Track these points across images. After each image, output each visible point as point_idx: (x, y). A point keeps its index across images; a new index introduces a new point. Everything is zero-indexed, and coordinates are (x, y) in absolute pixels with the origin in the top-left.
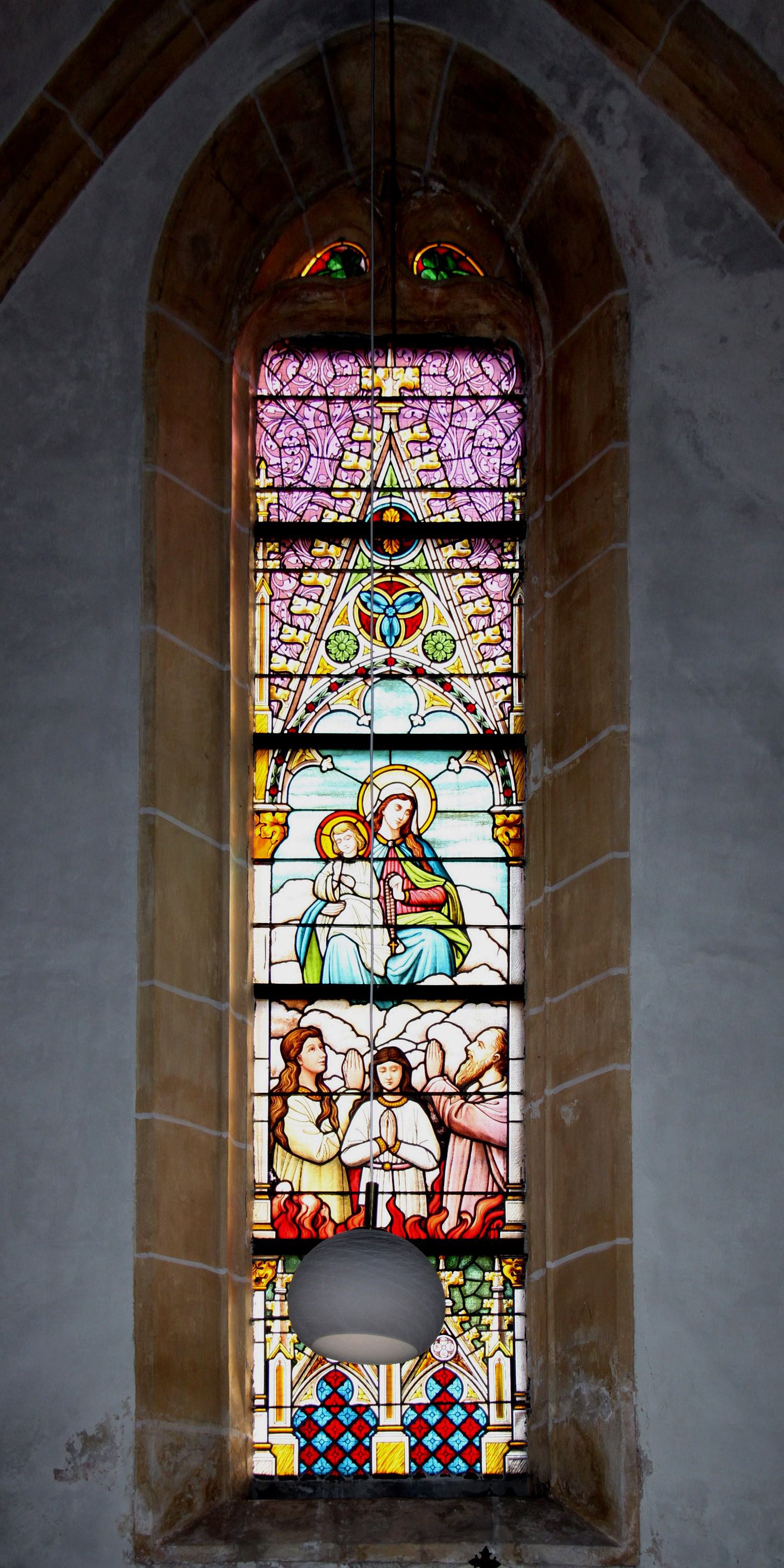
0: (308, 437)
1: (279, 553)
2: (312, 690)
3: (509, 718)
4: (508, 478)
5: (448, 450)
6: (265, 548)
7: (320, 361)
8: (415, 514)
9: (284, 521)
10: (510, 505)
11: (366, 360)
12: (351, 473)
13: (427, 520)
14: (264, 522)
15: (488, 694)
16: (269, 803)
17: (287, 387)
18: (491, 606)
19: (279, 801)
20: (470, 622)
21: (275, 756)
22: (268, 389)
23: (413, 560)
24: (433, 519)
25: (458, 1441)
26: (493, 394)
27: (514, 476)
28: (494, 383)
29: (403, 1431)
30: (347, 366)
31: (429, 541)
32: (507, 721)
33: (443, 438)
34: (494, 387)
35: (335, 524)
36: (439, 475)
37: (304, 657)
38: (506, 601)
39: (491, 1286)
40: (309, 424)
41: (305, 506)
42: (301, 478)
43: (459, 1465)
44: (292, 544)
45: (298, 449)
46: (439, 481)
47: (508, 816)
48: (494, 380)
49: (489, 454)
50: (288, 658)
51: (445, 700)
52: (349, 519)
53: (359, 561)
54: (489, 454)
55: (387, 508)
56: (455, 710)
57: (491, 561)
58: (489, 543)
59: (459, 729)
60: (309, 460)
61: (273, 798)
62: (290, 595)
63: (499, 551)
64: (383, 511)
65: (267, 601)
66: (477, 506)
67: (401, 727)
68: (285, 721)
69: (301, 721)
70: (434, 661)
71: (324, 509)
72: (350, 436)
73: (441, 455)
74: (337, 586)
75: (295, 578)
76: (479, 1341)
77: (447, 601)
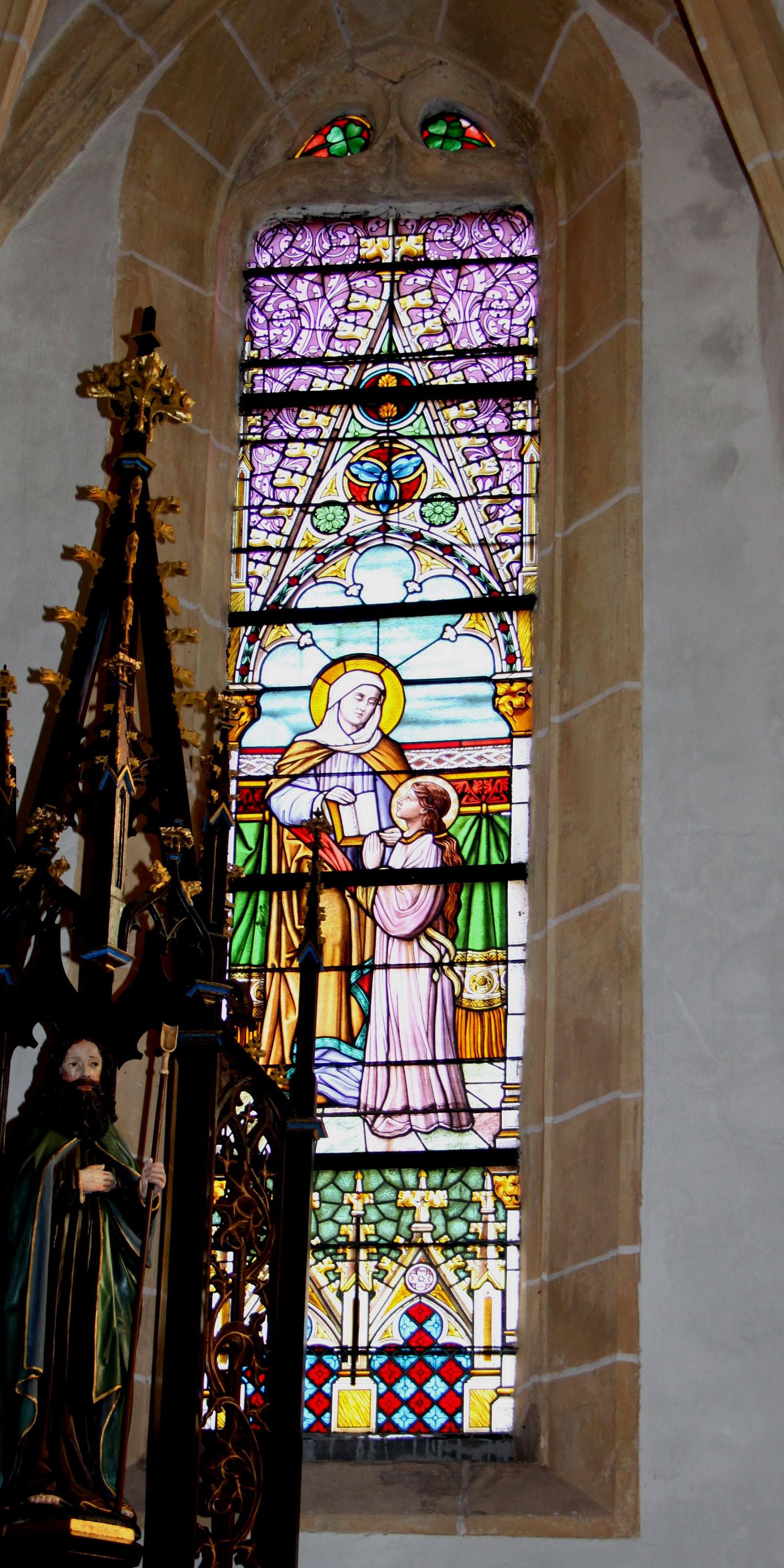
0: (300, 310)
1: (262, 426)
2: (295, 563)
3: (517, 579)
4: (519, 338)
5: (452, 314)
6: (246, 421)
7: (315, 231)
8: (415, 378)
9: (269, 392)
10: (521, 366)
11: (365, 229)
12: (345, 343)
13: (428, 384)
14: (247, 394)
15: (484, 527)
16: (238, 684)
17: (279, 261)
18: (499, 466)
19: (250, 681)
20: (475, 484)
21: (248, 633)
22: (257, 263)
23: (411, 424)
24: (434, 383)
25: (436, 1387)
26: (503, 256)
27: (526, 336)
28: (504, 245)
29: (371, 1376)
30: (344, 237)
31: (430, 404)
32: (515, 582)
33: (447, 304)
34: (504, 249)
35: (325, 392)
36: (440, 339)
37: (287, 530)
38: (516, 460)
39: (481, 1207)
40: (302, 297)
41: (292, 376)
42: (290, 350)
43: (436, 1418)
44: (275, 417)
45: (288, 321)
46: (442, 345)
47: (511, 685)
48: (505, 241)
49: (498, 316)
50: (269, 533)
51: (441, 567)
52: (341, 387)
53: (351, 429)
54: (498, 316)
55: (384, 374)
56: (458, 575)
57: (498, 423)
58: (497, 403)
59: (462, 594)
60: (300, 332)
61: (243, 678)
62: (272, 469)
63: (508, 410)
64: (379, 377)
65: (247, 476)
66: (484, 367)
67: (395, 596)
68: (264, 596)
69: (282, 595)
70: (431, 525)
71: (314, 377)
72: (345, 306)
73: (445, 320)
74: (325, 459)
75: (278, 451)
76: (464, 1271)
77: (449, 461)
